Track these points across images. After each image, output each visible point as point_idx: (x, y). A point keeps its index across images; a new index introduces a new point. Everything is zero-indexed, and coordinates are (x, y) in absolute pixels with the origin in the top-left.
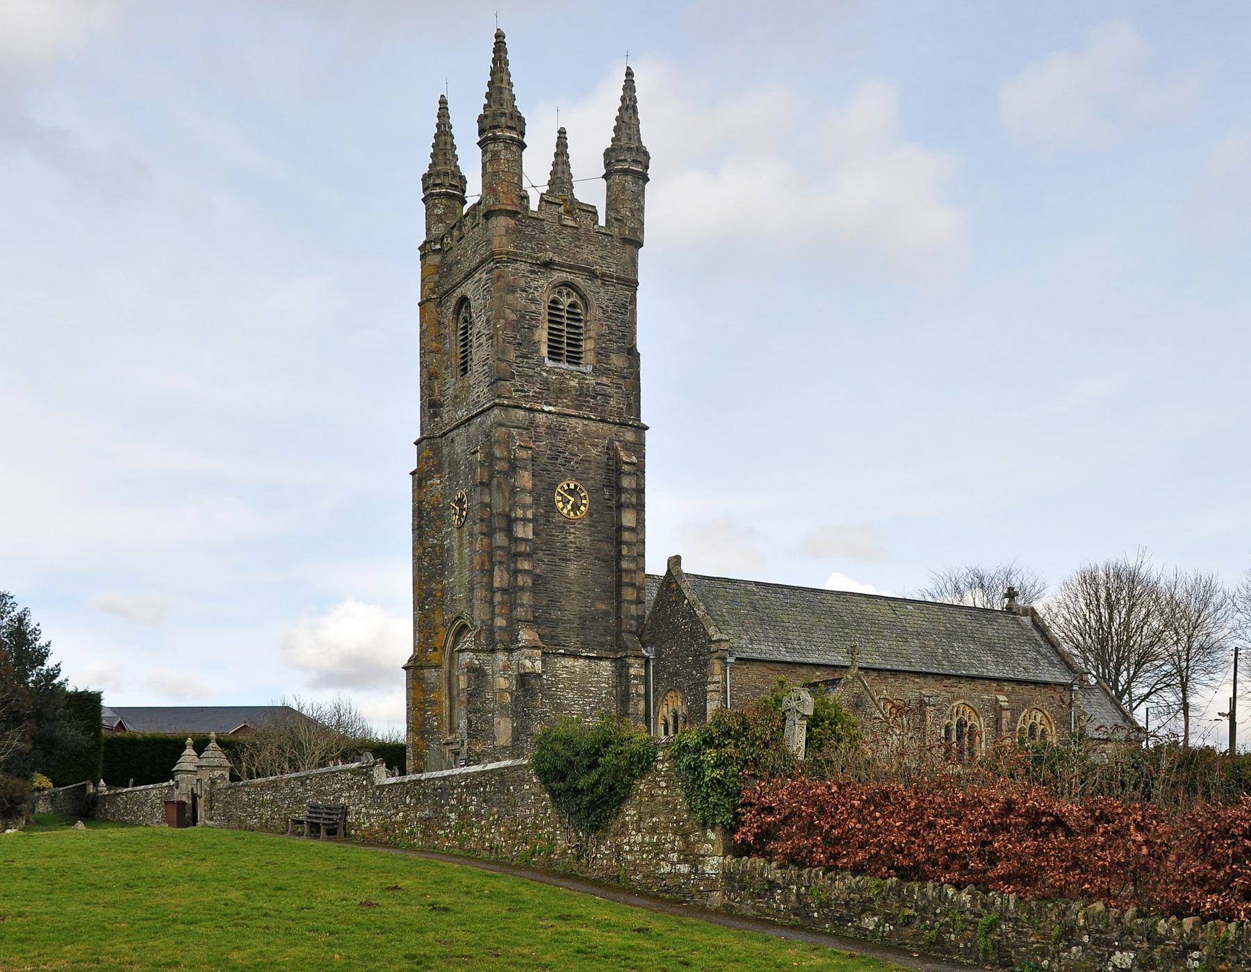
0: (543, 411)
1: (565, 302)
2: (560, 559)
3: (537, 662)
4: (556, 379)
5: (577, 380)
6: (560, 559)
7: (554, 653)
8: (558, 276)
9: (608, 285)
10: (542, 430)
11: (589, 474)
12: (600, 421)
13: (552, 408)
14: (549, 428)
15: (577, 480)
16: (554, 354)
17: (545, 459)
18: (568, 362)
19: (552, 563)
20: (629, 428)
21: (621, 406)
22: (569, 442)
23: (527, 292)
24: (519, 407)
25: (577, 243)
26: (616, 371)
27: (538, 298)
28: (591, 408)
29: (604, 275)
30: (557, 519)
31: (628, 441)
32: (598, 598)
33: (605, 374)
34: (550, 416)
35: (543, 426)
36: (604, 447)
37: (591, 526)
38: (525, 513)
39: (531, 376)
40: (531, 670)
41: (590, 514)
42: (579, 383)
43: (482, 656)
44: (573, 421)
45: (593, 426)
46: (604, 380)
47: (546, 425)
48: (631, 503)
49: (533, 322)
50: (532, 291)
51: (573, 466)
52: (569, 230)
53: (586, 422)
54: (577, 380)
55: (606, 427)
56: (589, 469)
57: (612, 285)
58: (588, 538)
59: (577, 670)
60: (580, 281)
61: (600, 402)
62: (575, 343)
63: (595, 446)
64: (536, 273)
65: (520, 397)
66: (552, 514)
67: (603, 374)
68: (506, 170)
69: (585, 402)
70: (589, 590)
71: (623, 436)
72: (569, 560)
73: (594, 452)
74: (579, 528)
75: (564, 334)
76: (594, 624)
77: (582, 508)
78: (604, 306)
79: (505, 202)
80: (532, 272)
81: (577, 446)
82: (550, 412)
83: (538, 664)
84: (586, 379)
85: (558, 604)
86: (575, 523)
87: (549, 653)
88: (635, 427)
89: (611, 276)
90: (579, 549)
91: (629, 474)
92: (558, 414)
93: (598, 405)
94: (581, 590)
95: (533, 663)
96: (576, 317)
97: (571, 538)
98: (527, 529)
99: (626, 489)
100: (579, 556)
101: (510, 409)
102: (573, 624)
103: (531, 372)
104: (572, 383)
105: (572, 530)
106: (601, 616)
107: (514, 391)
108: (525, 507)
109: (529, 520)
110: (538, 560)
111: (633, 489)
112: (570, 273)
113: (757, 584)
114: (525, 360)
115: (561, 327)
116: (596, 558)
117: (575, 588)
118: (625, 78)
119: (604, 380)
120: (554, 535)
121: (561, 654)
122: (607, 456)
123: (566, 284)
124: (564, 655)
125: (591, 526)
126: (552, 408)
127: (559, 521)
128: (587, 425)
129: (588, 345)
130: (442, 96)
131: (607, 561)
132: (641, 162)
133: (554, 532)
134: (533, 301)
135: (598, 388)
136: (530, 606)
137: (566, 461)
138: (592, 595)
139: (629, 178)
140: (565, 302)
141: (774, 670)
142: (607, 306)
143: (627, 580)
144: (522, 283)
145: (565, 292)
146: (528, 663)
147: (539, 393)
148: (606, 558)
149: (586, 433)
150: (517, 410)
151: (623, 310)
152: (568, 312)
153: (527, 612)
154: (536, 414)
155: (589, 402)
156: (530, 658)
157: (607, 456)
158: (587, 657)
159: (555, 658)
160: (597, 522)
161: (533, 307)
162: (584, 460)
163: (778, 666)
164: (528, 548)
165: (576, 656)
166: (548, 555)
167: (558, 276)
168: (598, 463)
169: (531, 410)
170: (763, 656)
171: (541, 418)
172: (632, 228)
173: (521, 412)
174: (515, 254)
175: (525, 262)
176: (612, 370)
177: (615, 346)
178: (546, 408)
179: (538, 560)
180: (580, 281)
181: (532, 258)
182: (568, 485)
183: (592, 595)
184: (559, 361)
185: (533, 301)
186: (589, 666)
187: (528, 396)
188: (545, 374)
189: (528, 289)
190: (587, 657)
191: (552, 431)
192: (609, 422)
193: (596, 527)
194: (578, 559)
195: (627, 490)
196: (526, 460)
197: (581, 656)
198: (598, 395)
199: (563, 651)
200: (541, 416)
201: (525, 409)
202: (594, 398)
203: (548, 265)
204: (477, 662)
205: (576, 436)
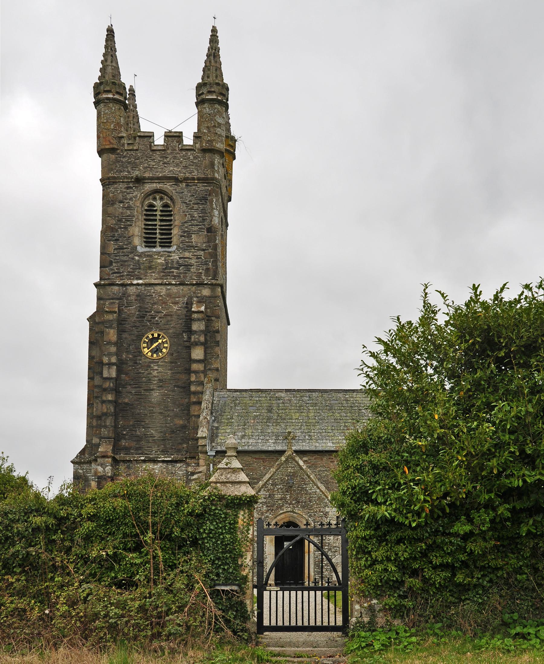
0: (132, 285)
1: (158, 204)
2: (145, 390)
3: (108, 468)
4: (146, 260)
5: (163, 259)
6: (145, 390)
7: (136, 460)
8: (149, 187)
9: (191, 186)
10: (133, 298)
11: (171, 325)
12: (180, 284)
13: (140, 282)
14: (138, 296)
15: (161, 330)
16: (149, 242)
17: (135, 319)
18: (160, 246)
19: (138, 394)
20: (205, 286)
21: (200, 271)
22: (155, 304)
23: (123, 202)
24: (113, 284)
25: (165, 160)
26: (196, 247)
27: (133, 205)
28: (174, 276)
29: (186, 179)
30: (143, 360)
31: (205, 296)
32: (176, 416)
33: (187, 250)
34: (139, 287)
35: (133, 295)
36: (183, 303)
37: (171, 363)
38: (110, 360)
39: (126, 261)
40: (102, 474)
41: (170, 354)
42: (165, 260)
43: (85, 466)
44: (158, 288)
45: (174, 289)
46: (187, 254)
47: (135, 294)
48: (199, 341)
49: (128, 223)
50: (128, 201)
51: (157, 321)
52: (158, 153)
53: (169, 287)
54: (163, 259)
55: (186, 288)
56: (172, 320)
57: (194, 185)
58: (170, 372)
59: (157, 471)
60: (168, 187)
61: (182, 271)
62: (167, 232)
63: (176, 303)
64: (131, 188)
65: (116, 277)
66: (139, 358)
67: (185, 250)
68: (105, 121)
69: (170, 272)
70: (169, 410)
71: (200, 293)
72: (153, 390)
73: (176, 308)
74: (162, 365)
75: (158, 227)
76: (173, 435)
77: (164, 350)
78: (187, 201)
79: (104, 143)
80: (128, 188)
81: (161, 305)
82: (138, 284)
83: (108, 468)
84: (171, 256)
85: (143, 423)
86: (158, 362)
87: (130, 461)
88: (209, 284)
89: (193, 179)
90: (160, 381)
91: (199, 320)
92: (146, 285)
93: (181, 273)
94: (161, 411)
95: (104, 469)
96: (168, 213)
97: (155, 373)
98: (111, 370)
99: (196, 332)
100: (161, 386)
101: (107, 287)
102: (155, 437)
103: (125, 258)
104: (159, 261)
105: (156, 368)
106: (179, 429)
107: (112, 274)
108: (110, 355)
109: (113, 364)
110: (127, 392)
111: (201, 331)
112: (159, 183)
113: (287, 391)
114: (121, 251)
115: (155, 223)
116: (175, 386)
117: (157, 410)
118: (211, 34)
119: (187, 254)
120: (140, 373)
121: (142, 460)
122: (186, 310)
123: (157, 191)
124: (144, 461)
125: (171, 363)
126: (140, 282)
127: (145, 362)
128: (169, 289)
129: (175, 231)
130: (131, 86)
131: (184, 388)
132: (214, 92)
133: (140, 371)
134: (129, 208)
135: (181, 261)
136: (112, 426)
137: (151, 318)
138: (171, 414)
139: (206, 105)
140: (158, 204)
141: (259, 459)
142: (190, 201)
143: (195, 400)
144: (120, 197)
145: (158, 197)
146: (100, 469)
147: (132, 272)
148: (183, 385)
149: (169, 295)
150: (112, 287)
151: (203, 202)
152: (161, 211)
153: (109, 431)
154: (128, 287)
155: (173, 272)
156: (102, 465)
157: (186, 310)
158: (163, 461)
159: (138, 463)
160: (177, 359)
161: (129, 212)
162: (167, 315)
163: (263, 456)
164: (111, 385)
165: (154, 461)
166: (135, 388)
167: (149, 187)
168: (178, 316)
169: (123, 285)
170: (253, 448)
171: (132, 290)
172: (209, 141)
173: (116, 288)
174: (114, 178)
175: (123, 182)
176: (193, 246)
177: (195, 228)
178: (135, 282)
179: (127, 392)
180: (168, 187)
181: (127, 178)
182: (153, 335)
183: (171, 414)
184: (154, 247)
185: (129, 208)
186: (166, 468)
187: (123, 276)
188: (137, 258)
189: (124, 200)
190: (163, 461)
191: (140, 297)
192: (187, 284)
193: (176, 363)
194: (160, 388)
195: (196, 332)
196: (112, 321)
197: (159, 462)
198: (181, 266)
199: (143, 458)
200: (132, 288)
201: (117, 285)
202: (178, 269)
203: (139, 181)
204: (81, 471)
205: (161, 298)
